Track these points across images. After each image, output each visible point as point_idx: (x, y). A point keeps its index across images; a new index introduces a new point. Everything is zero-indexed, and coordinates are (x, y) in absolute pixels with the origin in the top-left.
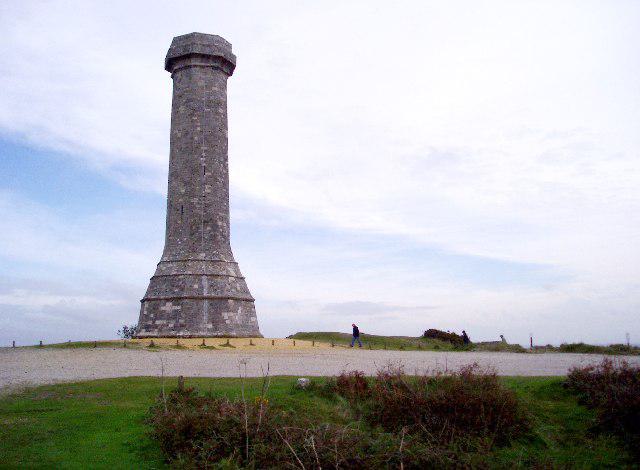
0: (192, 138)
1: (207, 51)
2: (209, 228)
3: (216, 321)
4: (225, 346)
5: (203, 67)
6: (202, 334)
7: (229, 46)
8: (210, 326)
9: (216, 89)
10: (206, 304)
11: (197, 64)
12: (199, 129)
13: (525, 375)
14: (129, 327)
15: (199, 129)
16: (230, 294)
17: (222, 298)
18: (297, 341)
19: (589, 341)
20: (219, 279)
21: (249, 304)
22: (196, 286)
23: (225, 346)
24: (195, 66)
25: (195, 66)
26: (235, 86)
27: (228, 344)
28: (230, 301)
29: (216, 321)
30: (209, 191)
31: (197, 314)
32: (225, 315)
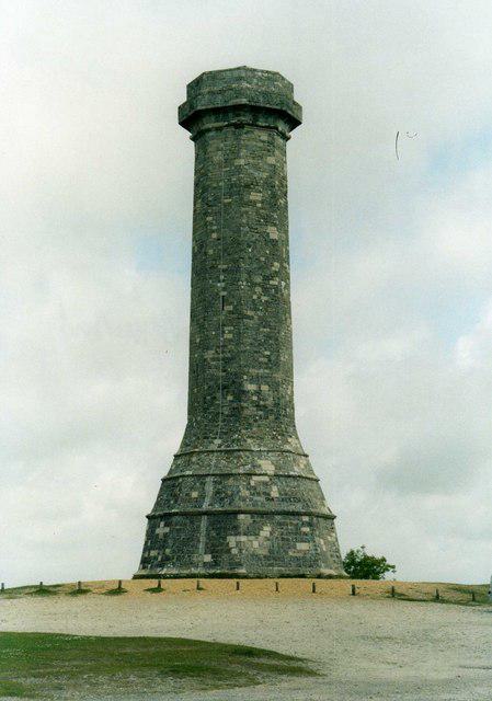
0: (206, 254)
1: (219, 102)
2: (230, 398)
3: (217, 549)
4: (153, 590)
5: (219, 129)
6: (194, 571)
7: (290, 87)
8: (208, 558)
9: (242, 162)
10: (204, 522)
11: (210, 126)
12: (214, 236)
13: (82, 634)
14: (387, 563)
15: (214, 236)
16: (242, 506)
17: (226, 513)
18: (282, 581)
19: (87, 576)
20: (231, 481)
21: (329, 522)
22: (195, 494)
23: (153, 590)
24: (209, 130)
25: (209, 130)
26: (300, 149)
27: (158, 590)
28: (241, 517)
29: (217, 549)
30: (230, 336)
31: (191, 541)
32: (232, 540)
